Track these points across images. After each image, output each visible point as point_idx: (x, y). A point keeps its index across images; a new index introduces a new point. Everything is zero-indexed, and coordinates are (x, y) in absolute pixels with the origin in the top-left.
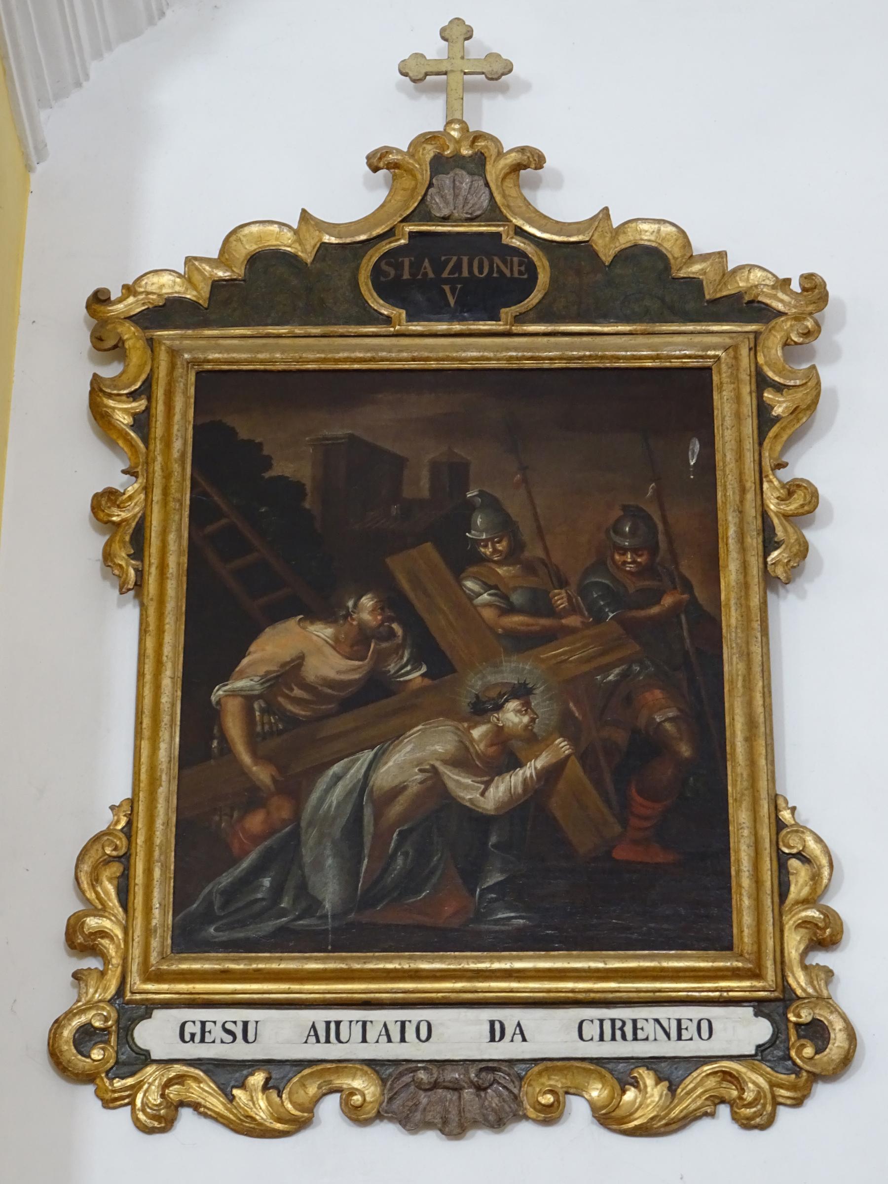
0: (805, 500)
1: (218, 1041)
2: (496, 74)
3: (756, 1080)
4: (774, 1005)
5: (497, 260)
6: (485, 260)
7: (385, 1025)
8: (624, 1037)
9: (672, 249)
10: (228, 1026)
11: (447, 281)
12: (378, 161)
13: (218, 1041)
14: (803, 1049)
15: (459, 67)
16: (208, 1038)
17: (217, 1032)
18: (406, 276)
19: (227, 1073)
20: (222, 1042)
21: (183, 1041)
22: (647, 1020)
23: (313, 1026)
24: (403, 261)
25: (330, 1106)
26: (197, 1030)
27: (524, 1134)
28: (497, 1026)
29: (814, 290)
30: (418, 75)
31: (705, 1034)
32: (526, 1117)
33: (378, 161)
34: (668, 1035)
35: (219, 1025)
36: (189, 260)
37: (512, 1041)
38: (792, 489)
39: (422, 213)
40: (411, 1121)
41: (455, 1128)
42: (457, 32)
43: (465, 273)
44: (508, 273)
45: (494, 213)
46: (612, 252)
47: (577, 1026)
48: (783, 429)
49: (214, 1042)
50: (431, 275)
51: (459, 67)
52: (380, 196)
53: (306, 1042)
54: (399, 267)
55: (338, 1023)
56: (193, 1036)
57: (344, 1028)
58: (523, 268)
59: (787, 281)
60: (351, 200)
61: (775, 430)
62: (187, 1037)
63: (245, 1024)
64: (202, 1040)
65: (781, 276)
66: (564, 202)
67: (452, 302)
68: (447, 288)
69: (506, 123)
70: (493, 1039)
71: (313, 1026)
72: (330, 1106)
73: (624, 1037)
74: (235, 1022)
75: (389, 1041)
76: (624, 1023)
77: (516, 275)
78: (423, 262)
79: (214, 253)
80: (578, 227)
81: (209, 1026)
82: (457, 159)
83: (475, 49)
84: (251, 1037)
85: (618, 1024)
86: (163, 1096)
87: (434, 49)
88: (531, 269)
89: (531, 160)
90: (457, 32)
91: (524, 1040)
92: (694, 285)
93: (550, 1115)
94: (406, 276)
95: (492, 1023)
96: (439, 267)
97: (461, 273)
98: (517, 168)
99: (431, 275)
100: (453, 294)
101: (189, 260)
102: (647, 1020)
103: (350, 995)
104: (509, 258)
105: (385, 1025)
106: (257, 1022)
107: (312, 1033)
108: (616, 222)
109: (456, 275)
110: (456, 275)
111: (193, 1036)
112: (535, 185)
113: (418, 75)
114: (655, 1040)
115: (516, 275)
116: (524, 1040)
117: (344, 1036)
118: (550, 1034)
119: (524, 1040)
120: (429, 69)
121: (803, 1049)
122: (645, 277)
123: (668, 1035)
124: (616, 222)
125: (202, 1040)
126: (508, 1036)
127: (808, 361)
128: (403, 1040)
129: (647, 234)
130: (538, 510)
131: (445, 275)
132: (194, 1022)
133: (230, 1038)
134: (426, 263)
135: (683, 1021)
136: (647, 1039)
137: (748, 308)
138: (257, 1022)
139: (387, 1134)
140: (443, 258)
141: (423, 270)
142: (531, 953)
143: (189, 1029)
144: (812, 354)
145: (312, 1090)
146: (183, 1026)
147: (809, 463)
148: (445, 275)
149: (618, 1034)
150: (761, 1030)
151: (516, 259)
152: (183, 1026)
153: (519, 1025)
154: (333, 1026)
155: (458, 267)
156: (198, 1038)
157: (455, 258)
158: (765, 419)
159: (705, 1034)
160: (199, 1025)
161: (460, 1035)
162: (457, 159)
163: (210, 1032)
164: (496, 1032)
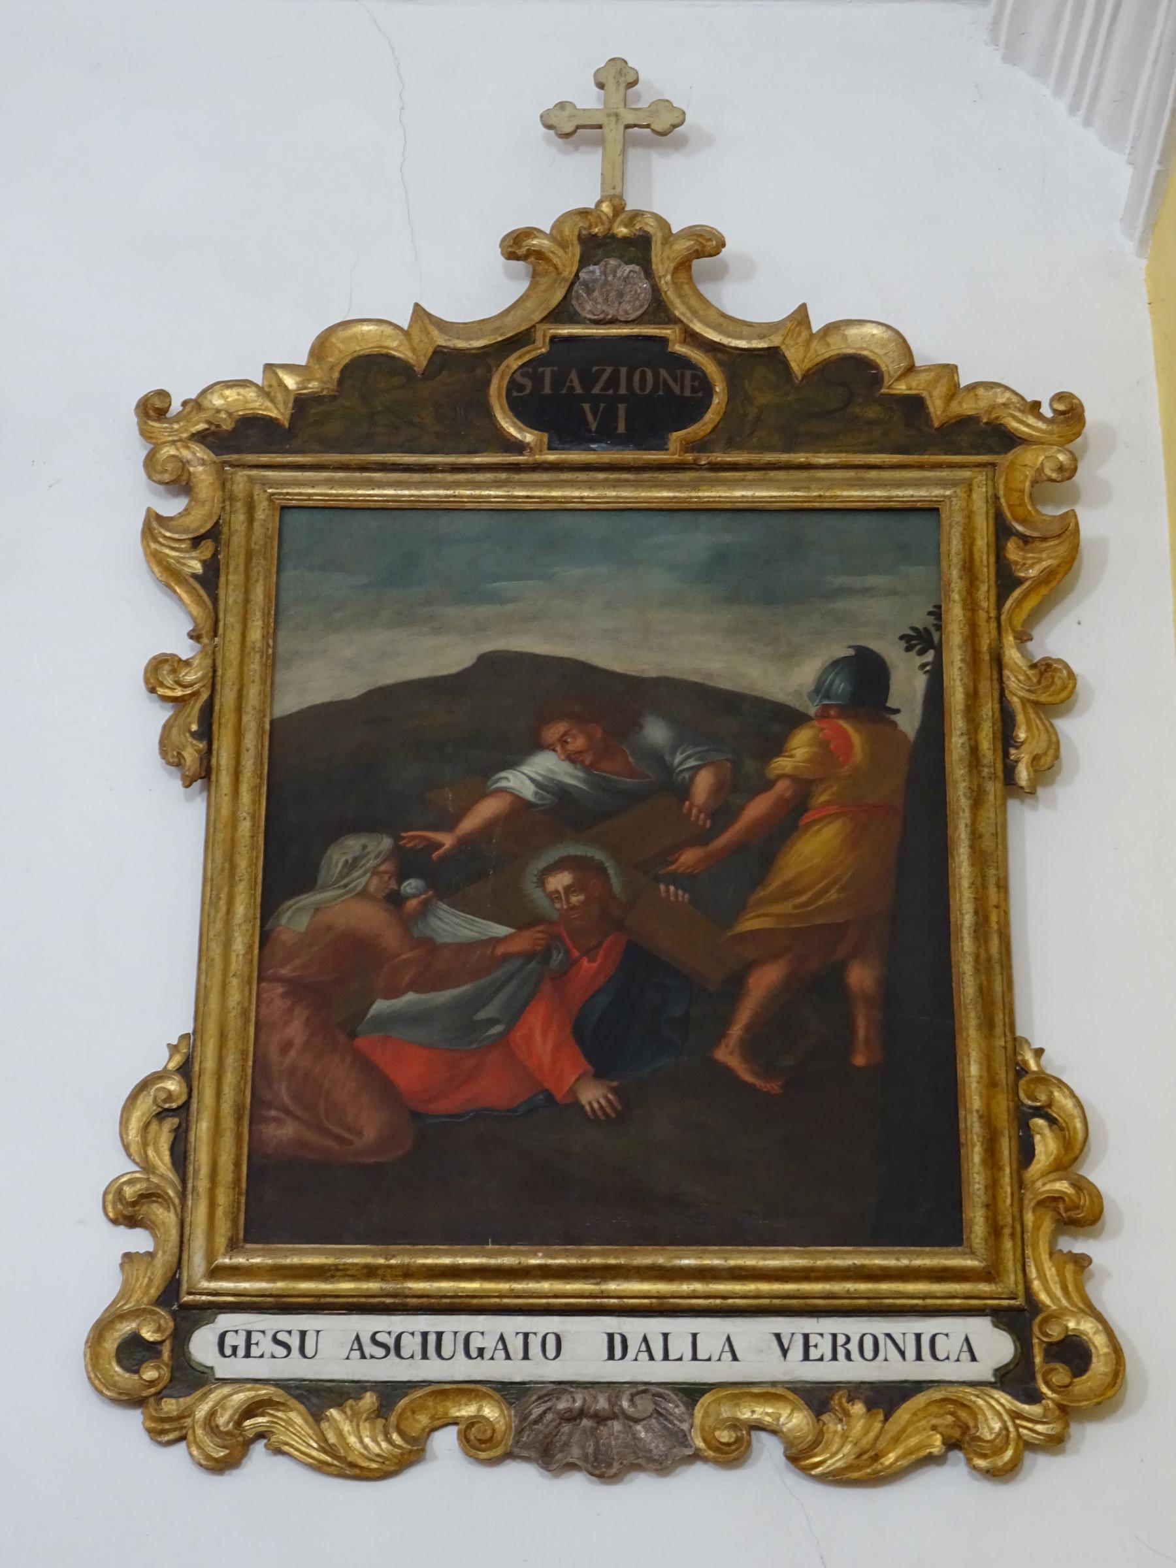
0: (1055, 686)
1: (267, 1355)
2: (663, 129)
3: (994, 1413)
4: (1018, 1318)
5: (663, 372)
6: (649, 374)
7: (502, 1338)
8: (848, 1356)
9: (889, 364)
10: (280, 1337)
11: (595, 400)
12: (517, 246)
13: (267, 1355)
14: (1060, 1373)
15: (624, 118)
16: (254, 1351)
17: (265, 1345)
18: (547, 390)
19: (318, 1397)
20: (273, 1357)
21: (304, 1356)
22: (821, 1335)
23: (357, 1338)
24: (543, 373)
25: (445, 1441)
26: (240, 1341)
27: (699, 1481)
28: (618, 1340)
29: (1070, 414)
30: (569, 129)
31: (551, 1352)
32: (697, 1457)
33: (517, 246)
34: (902, 1354)
35: (270, 1335)
36: (269, 368)
37: (958, 1360)
38: (1046, 669)
39: (562, 313)
40: (548, 1454)
41: (605, 1467)
42: (618, 77)
43: (623, 391)
44: (677, 390)
45: (658, 310)
46: (807, 365)
47: (216, 1340)
48: (1025, 596)
49: (262, 1356)
50: (579, 390)
51: (624, 118)
52: (520, 287)
53: (636, 1360)
54: (538, 380)
55: (440, 1335)
56: (235, 1348)
57: (447, 1340)
58: (696, 384)
59: (1036, 405)
60: (477, 292)
61: (1016, 593)
62: (228, 1351)
63: (303, 1334)
64: (248, 1355)
65: (1029, 399)
66: (751, 297)
67: (594, 427)
68: (586, 407)
69: (672, 195)
70: (611, 1356)
71: (357, 1338)
72: (445, 1441)
73: (848, 1356)
74: (290, 1332)
75: (652, 1358)
76: (848, 1339)
77: (687, 393)
78: (569, 373)
79: (301, 358)
80: (773, 327)
81: (255, 1338)
82: (613, 242)
83: (645, 95)
84: (309, 1351)
85: (841, 1340)
86: (239, 1424)
87: (588, 99)
88: (705, 386)
89: (706, 244)
90: (618, 77)
91: (735, 1358)
92: (915, 405)
93: (732, 1453)
94: (547, 390)
95: (611, 1336)
96: (588, 380)
97: (617, 388)
98: (684, 265)
99: (579, 390)
100: (595, 415)
101: (269, 368)
102: (821, 1335)
103: (801, 1301)
104: (679, 372)
105: (502, 1338)
106: (318, 1332)
107: (644, 1348)
108: (816, 325)
109: (611, 392)
110: (611, 392)
111: (235, 1348)
112: (719, 275)
113: (569, 129)
114: (886, 1360)
115: (687, 393)
116: (735, 1358)
117: (446, 1352)
118: (754, 1349)
119: (735, 1358)
120: (580, 122)
121: (1060, 1373)
122: (849, 397)
123: (902, 1354)
124: (816, 325)
125: (248, 1355)
126: (631, 1353)
127: (1058, 503)
128: (526, 1357)
129: (859, 340)
130: (1012, 683)
131: (596, 390)
132: (413, 1334)
133: (284, 1352)
134: (574, 375)
135: (811, 1337)
136: (821, 1359)
137: (984, 435)
138: (318, 1332)
139: (522, 1476)
140: (595, 369)
141: (568, 384)
142: (851, 1248)
143: (230, 1340)
144: (1075, 497)
145: (423, 1420)
146: (222, 1337)
147: (1061, 638)
148: (596, 390)
149: (841, 1352)
150: (202, 1346)
151: (688, 374)
152: (222, 1337)
153: (967, 1339)
154: (432, 1339)
155: (613, 381)
156: (241, 1352)
157: (609, 370)
158: (1006, 581)
159: (551, 1352)
160: (243, 1335)
161: (582, 1351)
162: (613, 242)
163: (816, 1346)
164: (615, 1347)
